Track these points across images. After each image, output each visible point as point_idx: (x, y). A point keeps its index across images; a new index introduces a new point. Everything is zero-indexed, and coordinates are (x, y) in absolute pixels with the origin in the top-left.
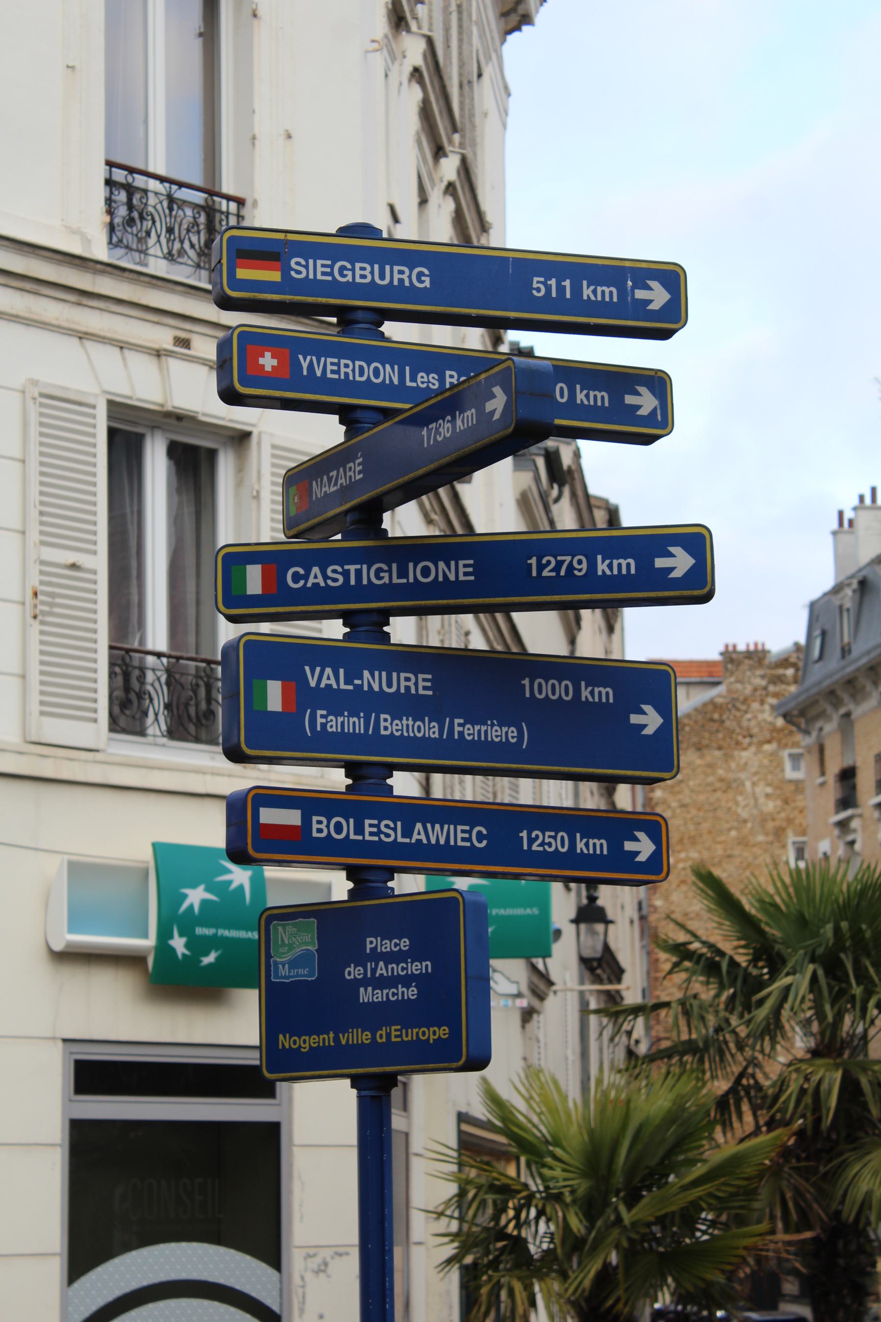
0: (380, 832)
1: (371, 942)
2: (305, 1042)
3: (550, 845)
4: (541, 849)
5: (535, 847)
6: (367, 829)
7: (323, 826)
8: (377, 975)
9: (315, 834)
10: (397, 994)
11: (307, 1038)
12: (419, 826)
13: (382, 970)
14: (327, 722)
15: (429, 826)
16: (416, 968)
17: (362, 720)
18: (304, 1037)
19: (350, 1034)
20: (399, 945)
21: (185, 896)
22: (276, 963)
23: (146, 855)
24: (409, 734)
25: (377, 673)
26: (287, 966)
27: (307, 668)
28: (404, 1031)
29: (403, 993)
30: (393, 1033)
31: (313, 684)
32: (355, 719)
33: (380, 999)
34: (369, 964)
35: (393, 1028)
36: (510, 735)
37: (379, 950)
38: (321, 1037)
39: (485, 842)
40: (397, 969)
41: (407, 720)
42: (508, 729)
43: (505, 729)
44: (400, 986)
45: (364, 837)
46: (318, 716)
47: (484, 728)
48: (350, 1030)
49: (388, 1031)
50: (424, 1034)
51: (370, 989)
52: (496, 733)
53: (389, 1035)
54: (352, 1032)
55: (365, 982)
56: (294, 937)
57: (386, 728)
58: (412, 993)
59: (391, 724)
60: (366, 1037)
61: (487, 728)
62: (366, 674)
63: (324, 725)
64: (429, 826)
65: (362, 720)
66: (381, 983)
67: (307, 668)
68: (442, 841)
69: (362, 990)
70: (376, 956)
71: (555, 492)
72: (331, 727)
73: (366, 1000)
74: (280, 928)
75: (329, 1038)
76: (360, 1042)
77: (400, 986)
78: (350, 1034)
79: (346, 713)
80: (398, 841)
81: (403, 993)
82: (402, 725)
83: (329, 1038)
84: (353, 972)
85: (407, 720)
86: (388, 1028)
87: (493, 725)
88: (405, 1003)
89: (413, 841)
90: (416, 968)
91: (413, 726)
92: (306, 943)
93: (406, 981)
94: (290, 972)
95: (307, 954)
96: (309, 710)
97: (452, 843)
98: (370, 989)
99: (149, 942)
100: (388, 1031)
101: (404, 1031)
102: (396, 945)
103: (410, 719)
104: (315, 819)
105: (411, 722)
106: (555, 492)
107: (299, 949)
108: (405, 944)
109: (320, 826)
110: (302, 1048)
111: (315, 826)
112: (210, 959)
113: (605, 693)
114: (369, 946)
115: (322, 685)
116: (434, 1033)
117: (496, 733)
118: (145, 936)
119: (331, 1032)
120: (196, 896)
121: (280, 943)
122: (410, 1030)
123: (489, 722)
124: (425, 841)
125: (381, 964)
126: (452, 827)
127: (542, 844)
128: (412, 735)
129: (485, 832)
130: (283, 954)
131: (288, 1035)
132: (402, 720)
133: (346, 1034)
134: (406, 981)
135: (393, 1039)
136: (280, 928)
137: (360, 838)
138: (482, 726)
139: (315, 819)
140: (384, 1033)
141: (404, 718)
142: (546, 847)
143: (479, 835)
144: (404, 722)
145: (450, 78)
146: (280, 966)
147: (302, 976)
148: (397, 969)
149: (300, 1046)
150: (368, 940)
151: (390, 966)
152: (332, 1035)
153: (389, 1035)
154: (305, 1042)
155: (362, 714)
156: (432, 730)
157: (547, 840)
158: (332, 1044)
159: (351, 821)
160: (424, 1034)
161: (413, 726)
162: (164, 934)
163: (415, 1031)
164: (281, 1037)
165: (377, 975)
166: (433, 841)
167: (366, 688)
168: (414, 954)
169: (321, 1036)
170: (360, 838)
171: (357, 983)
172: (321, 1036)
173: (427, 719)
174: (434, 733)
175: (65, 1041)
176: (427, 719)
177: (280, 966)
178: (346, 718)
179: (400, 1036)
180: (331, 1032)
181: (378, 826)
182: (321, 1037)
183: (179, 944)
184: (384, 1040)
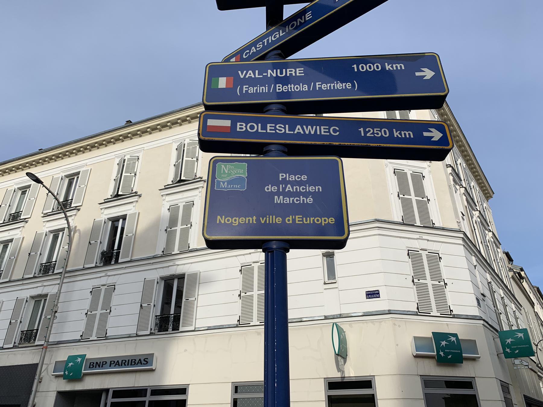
0: (276, 129)
1: (282, 176)
2: (235, 220)
3: (378, 134)
4: (373, 135)
5: (368, 135)
6: (268, 128)
7: (281, 88)
8: (286, 191)
9: (238, 130)
10: (300, 200)
11: (237, 219)
12: (299, 127)
13: (289, 188)
14: (249, 90)
15: (305, 127)
16: (311, 189)
17: (267, 87)
18: (235, 218)
19: (268, 219)
20: (301, 178)
21: (441, 343)
22: (219, 182)
23: (431, 335)
24: (291, 90)
25: (275, 71)
26: (226, 183)
27: (240, 72)
28: (304, 219)
29: (303, 200)
30: (297, 219)
31: (242, 77)
32: (264, 88)
33: (252, 92)
34: (281, 186)
35: (297, 217)
36: (347, 86)
37: (288, 179)
38: (247, 219)
39: (338, 133)
40: (301, 189)
41: (291, 85)
42: (346, 84)
43: (344, 84)
44: (301, 197)
45: (267, 131)
46: (244, 88)
47: (332, 85)
48: (268, 216)
49: (294, 218)
50: (318, 220)
51: (281, 197)
52: (366, 68)
53: (294, 220)
54: (269, 217)
55: (278, 194)
56: (232, 170)
57: (279, 89)
58: (310, 200)
59: (282, 88)
60: (279, 220)
61: (335, 84)
62: (269, 71)
63: (246, 91)
64: (305, 127)
65: (267, 87)
66: (290, 194)
67: (240, 72)
68: (312, 133)
69: (276, 197)
70: (285, 182)
71: (522, 281)
72: (251, 91)
73: (279, 202)
74: (223, 166)
75: (253, 220)
76: (274, 222)
77: (301, 197)
78: (268, 219)
79: (258, 86)
80: (287, 132)
81: (303, 200)
82: (288, 87)
83: (253, 220)
84: (270, 188)
85: (291, 85)
86: (294, 216)
87: (337, 83)
88: (304, 205)
89: (295, 132)
90: (311, 189)
91: (294, 87)
92: (241, 174)
93: (306, 195)
94: (227, 186)
95: (241, 178)
96: (239, 86)
97: (318, 133)
98: (281, 197)
99: (435, 353)
100: (294, 218)
101: (304, 219)
102: (298, 178)
103: (292, 85)
104: (277, 85)
105: (292, 86)
106: (522, 281)
107: (235, 176)
108: (304, 178)
109: (279, 88)
110: (233, 223)
111: (277, 88)
112: (450, 356)
113: (400, 66)
114: (281, 178)
115: (247, 77)
116: (325, 220)
117: (366, 68)
118: (434, 352)
119: (254, 217)
120: (444, 343)
121: (222, 172)
122: (271, 222)
123: (335, 82)
124: (302, 133)
125: (289, 186)
126: (318, 127)
127: (373, 133)
128: (293, 90)
129: (337, 129)
130: (224, 177)
131: (223, 217)
132: (288, 85)
133: (265, 218)
134: (306, 195)
135: (297, 222)
136: (223, 166)
137: (265, 131)
138: (332, 84)
139: (277, 85)
140: (291, 219)
141: (289, 85)
142: (376, 135)
143: (335, 131)
144: (289, 86)
145: (487, 220)
146: (221, 183)
147: (235, 188)
148: (301, 189)
149: (232, 222)
150: (280, 175)
151: (295, 187)
152: (254, 218)
153: (294, 220)
154: (235, 220)
155: (267, 85)
156: (304, 88)
157: (375, 132)
158: (255, 222)
159: (260, 125)
160: (318, 220)
161: (294, 87)
162: (438, 352)
163: (312, 219)
164: (219, 217)
165: (286, 191)
166: (307, 132)
167: (269, 76)
168: (310, 182)
169: (247, 218)
170: (265, 131)
171: (272, 194)
172: (247, 218)
173: (301, 84)
174: (305, 89)
175: (420, 375)
176: (301, 84)
177: (221, 183)
178: (258, 88)
179: (302, 221)
180: (254, 217)
181: (275, 127)
182: (247, 219)
183: (442, 353)
184: (291, 222)
